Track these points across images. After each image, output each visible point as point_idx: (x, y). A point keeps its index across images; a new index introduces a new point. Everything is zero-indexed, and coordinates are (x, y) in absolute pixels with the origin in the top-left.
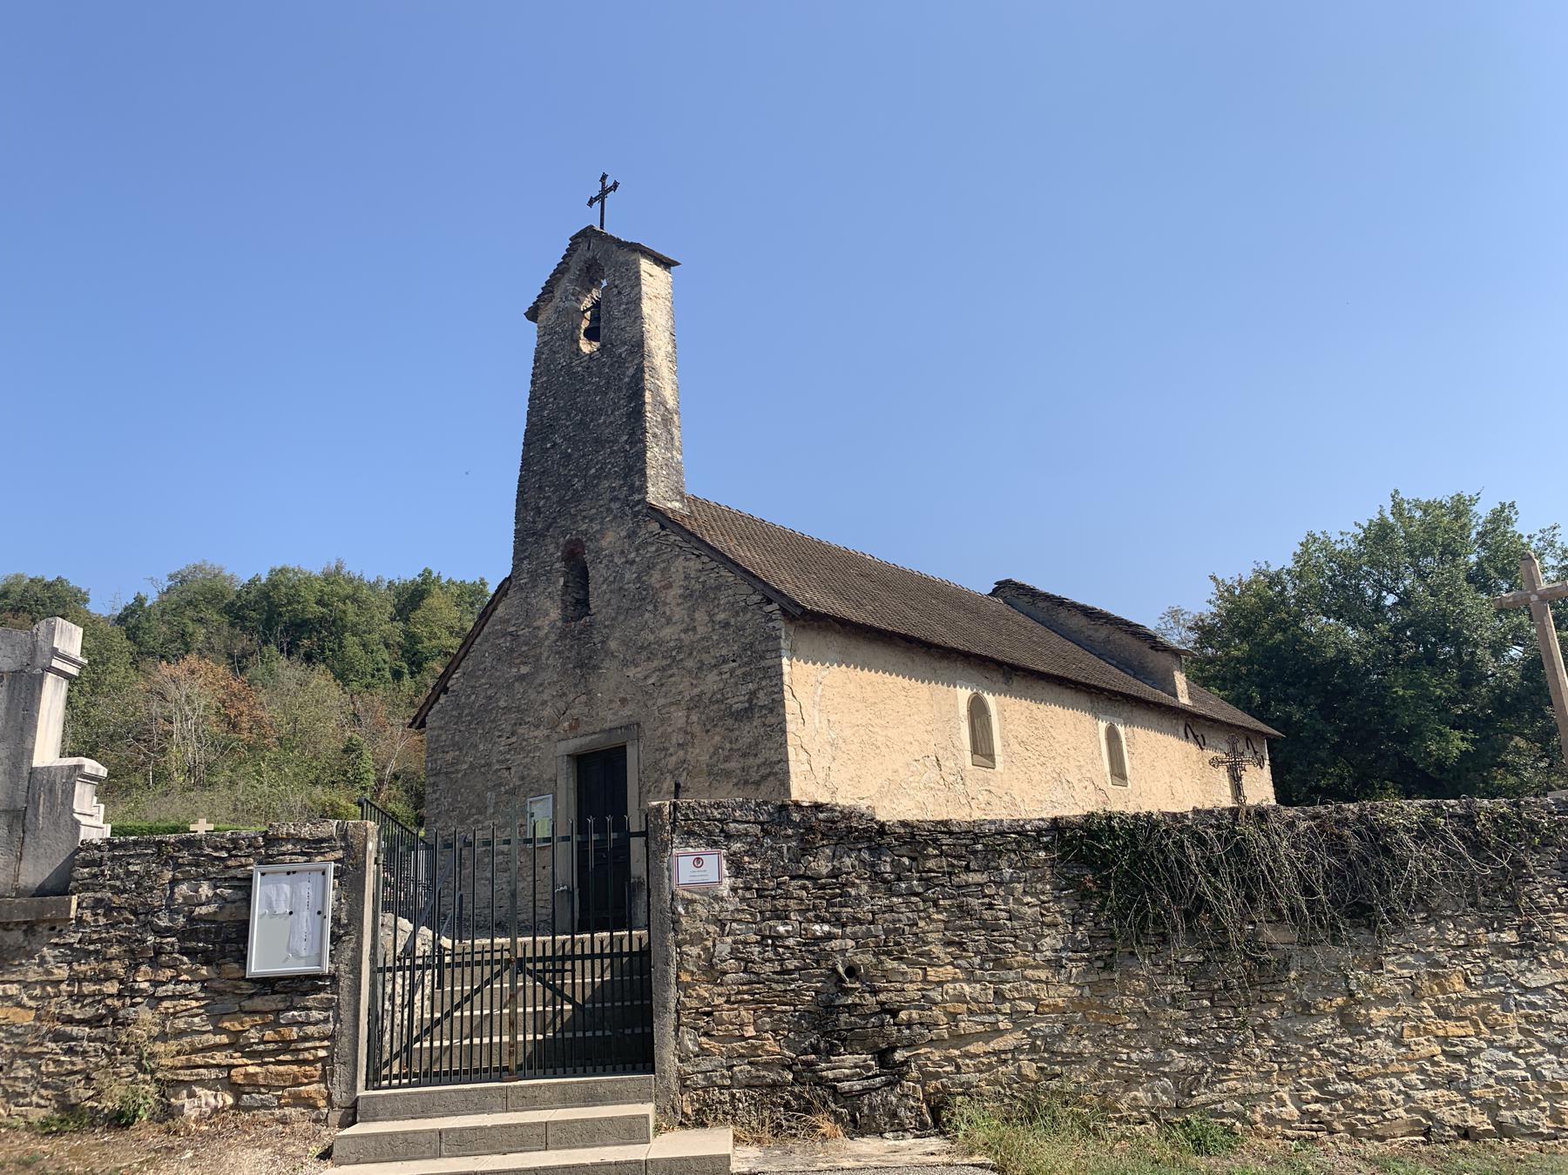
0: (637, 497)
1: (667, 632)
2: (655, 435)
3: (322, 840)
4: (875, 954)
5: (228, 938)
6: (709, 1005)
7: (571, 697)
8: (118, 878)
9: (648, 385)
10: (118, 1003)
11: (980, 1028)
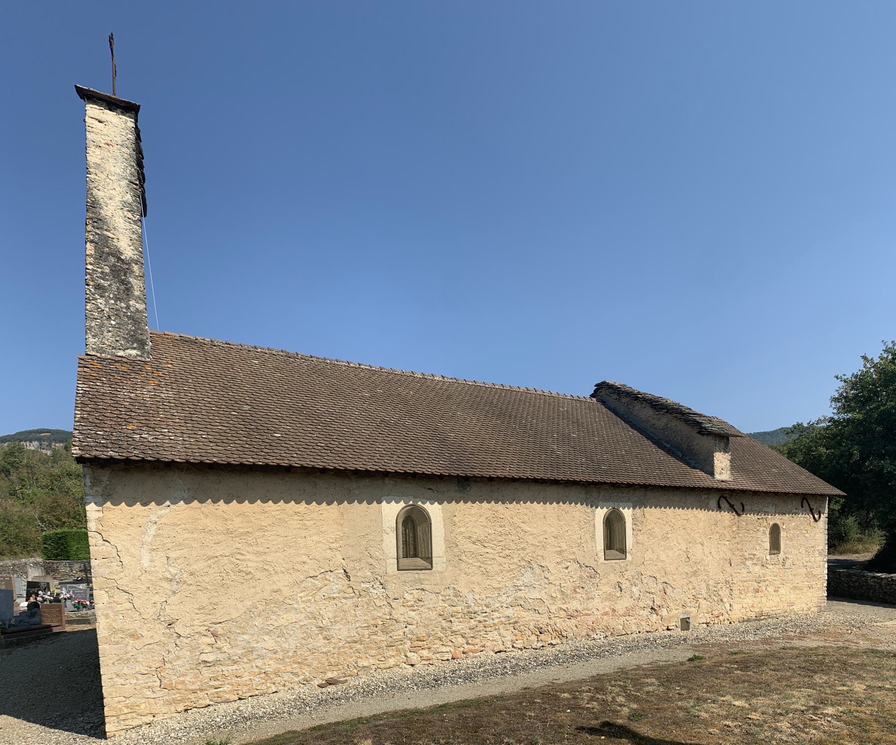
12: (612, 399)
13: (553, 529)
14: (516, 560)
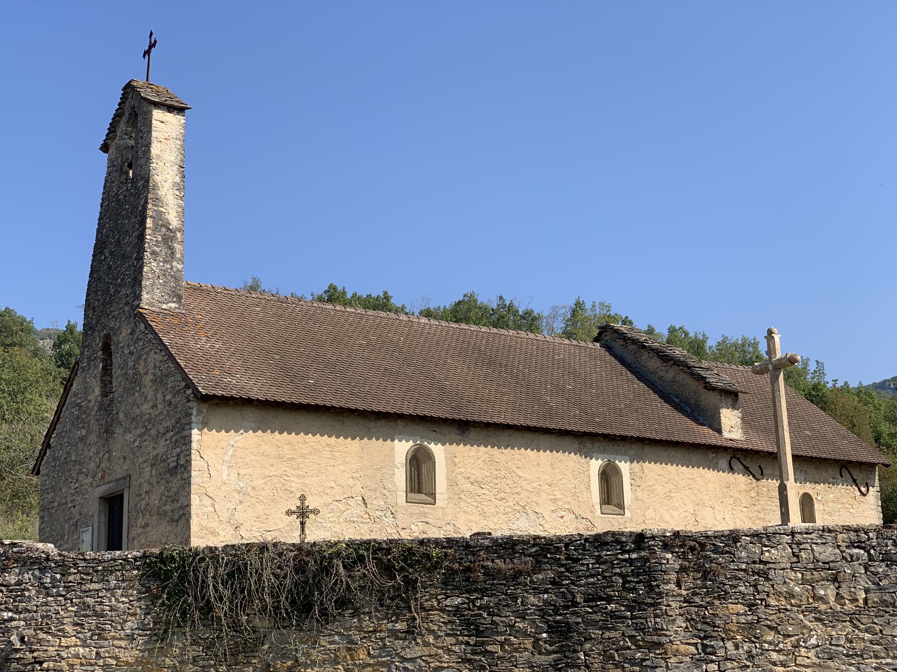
2: (153, 253)
4: (35, 630)
12: (618, 345)
13: (547, 477)
14: (511, 504)
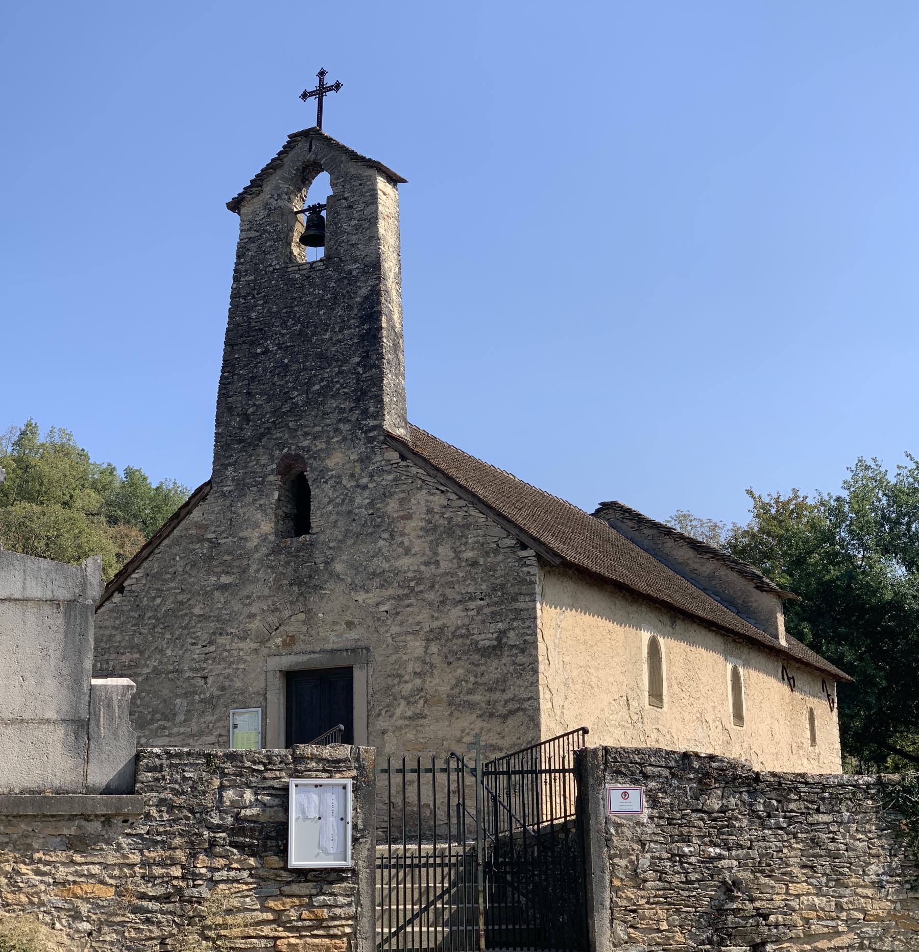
0: (371, 423)
1: (404, 562)
3: (339, 761)
4: (753, 872)
5: (273, 836)
6: (634, 904)
7: (287, 613)
8: (176, 782)
9: (384, 310)
10: (183, 884)
11: (826, 930)
